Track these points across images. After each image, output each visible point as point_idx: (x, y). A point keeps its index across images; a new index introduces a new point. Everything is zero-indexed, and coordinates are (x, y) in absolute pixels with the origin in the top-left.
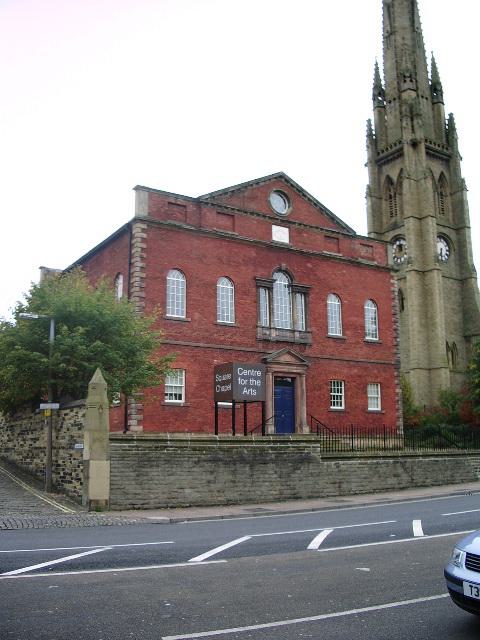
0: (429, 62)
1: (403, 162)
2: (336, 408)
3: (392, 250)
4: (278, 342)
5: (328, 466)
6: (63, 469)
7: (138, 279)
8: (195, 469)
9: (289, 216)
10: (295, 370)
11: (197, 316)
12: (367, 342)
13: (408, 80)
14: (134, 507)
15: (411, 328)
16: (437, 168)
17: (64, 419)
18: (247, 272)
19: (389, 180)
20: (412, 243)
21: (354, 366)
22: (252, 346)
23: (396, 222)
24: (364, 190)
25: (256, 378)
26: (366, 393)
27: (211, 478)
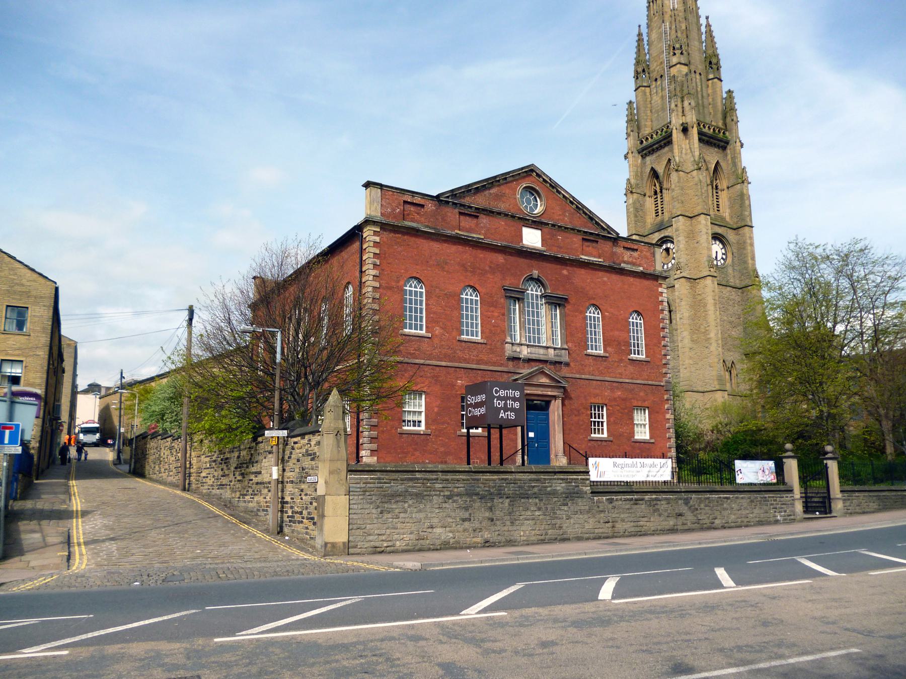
0: (703, 21)
1: (672, 151)
2: (597, 435)
3: (659, 252)
6: (292, 507)
7: (370, 289)
8: (447, 505)
10: (550, 393)
11: (438, 330)
13: (678, 52)
14: (377, 551)
15: (680, 345)
16: (713, 156)
17: (293, 448)
18: (495, 282)
19: (654, 174)
20: (682, 246)
21: (618, 388)
22: (501, 365)
23: (662, 222)
25: (514, 399)
26: (632, 419)
27: (466, 515)
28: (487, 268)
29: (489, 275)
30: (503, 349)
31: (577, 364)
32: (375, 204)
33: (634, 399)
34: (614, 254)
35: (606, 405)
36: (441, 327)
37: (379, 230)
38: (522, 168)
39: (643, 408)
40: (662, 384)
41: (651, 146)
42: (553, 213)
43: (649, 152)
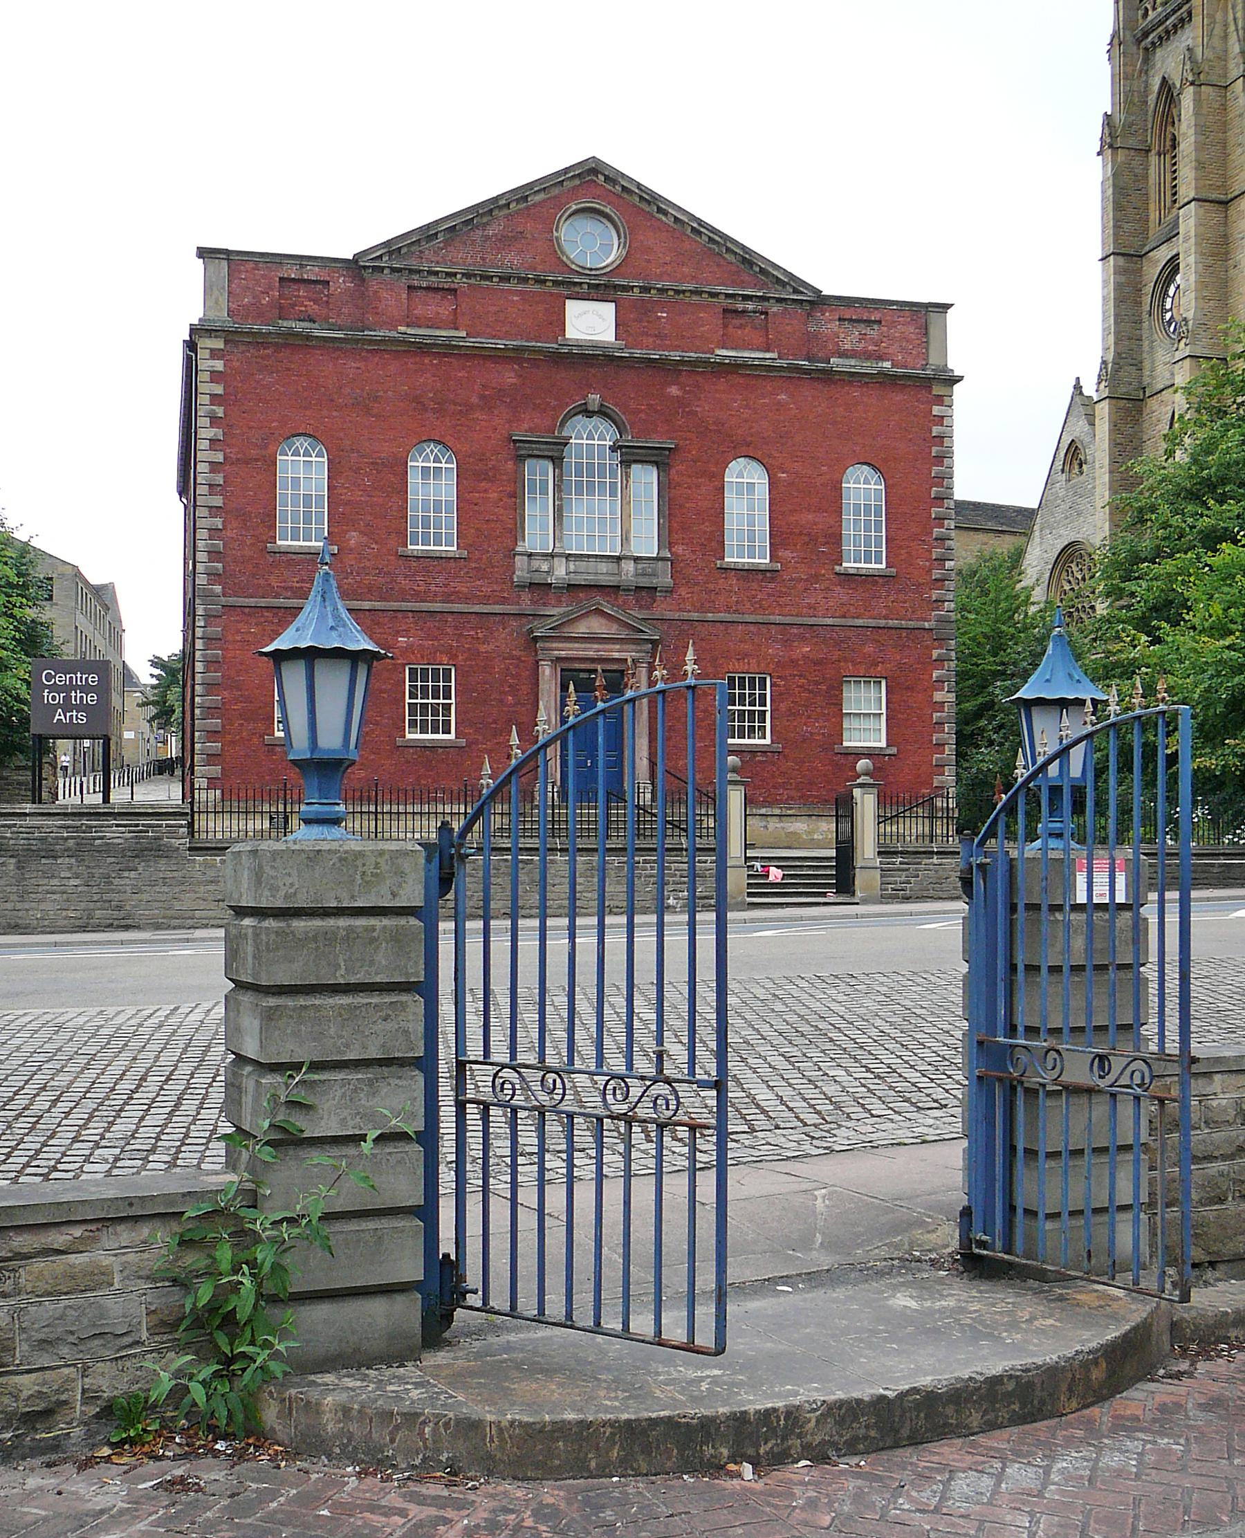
2: (736, 741)
4: (571, 587)
5: (205, 863)
9: (617, 270)
12: (850, 578)
21: (802, 638)
22: (504, 601)
24: (1095, 130)
25: (86, 689)
28: (474, 400)
29: (478, 415)
30: (511, 568)
31: (696, 589)
32: (216, 292)
33: (845, 660)
34: (811, 338)
35: (770, 675)
36: (361, 532)
37: (222, 346)
38: (566, 170)
39: (871, 678)
40: (927, 625)
41: (1161, 23)
42: (649, 261)
43: (1167, 32)
